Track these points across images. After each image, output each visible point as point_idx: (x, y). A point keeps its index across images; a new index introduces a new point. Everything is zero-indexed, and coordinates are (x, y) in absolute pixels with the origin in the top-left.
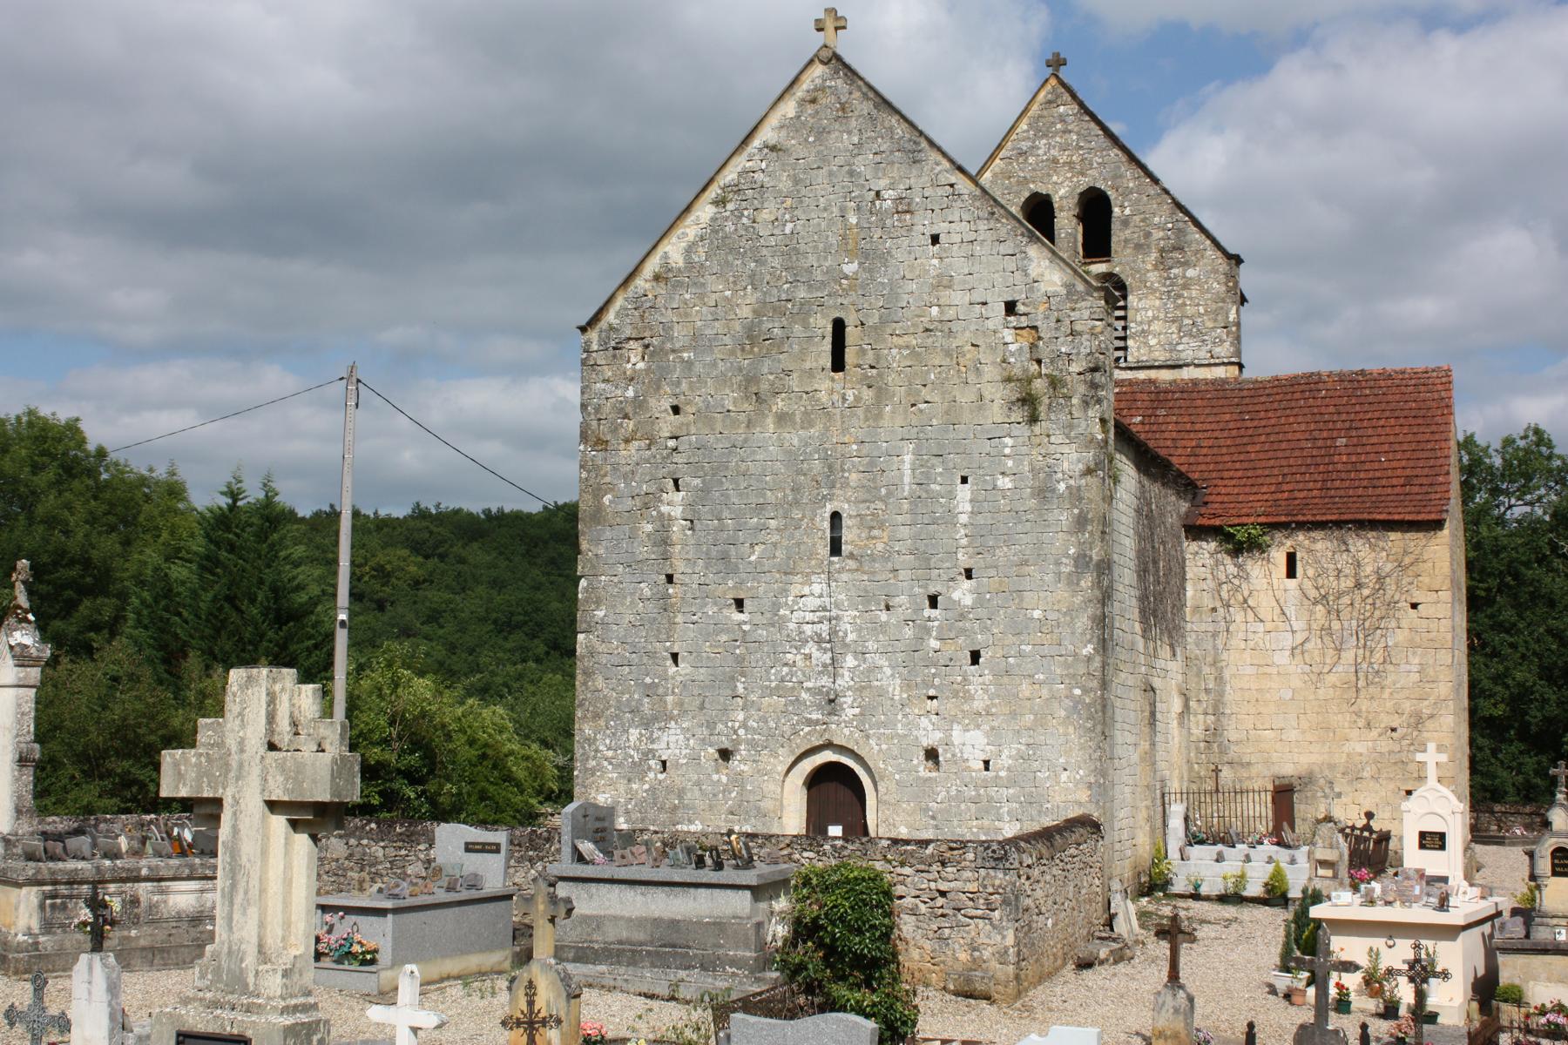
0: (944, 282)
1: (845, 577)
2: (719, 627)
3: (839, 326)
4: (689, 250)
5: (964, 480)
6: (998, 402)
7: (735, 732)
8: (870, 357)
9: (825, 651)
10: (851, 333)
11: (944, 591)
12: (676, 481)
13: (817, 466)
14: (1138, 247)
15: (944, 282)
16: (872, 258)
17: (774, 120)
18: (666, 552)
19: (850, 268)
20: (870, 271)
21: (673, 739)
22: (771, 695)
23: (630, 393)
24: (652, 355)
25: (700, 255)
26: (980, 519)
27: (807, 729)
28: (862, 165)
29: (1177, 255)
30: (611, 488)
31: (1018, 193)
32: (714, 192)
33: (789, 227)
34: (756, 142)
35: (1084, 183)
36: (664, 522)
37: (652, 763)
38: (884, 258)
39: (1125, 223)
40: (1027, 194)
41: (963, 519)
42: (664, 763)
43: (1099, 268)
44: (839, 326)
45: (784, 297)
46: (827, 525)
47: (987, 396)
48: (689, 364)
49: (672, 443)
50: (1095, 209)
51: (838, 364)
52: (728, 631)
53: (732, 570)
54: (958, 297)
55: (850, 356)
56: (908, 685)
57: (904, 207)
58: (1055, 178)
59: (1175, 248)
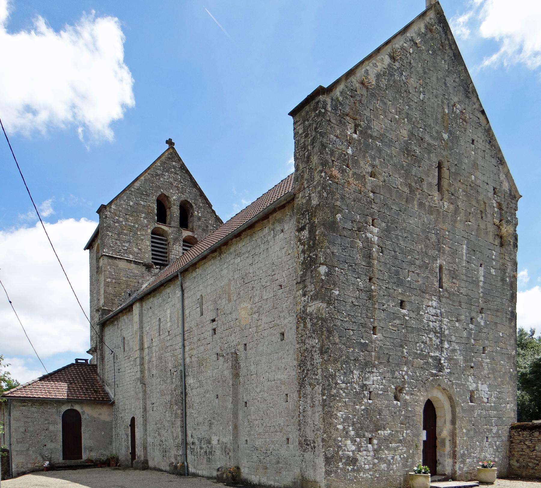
2: (395, 316)
4: (378, 76)
9: (438, 337)
11: (475, 316)
13: (434, 238)
21: (375, 378)
22: (417, 358)
24: (361, 132)
27: (431, 378)
28: (450, 81)
30: (340, 211)
31: (156, 191)
32: (388, 49)
34: (408, 34)
35: (183, 197)
36: (368, 242)
37: (365, 392)
39: (199, 219)
40: (160, 193)
41: (481, 284)
43: (186, 233)
46: (438, 270)
48: (380, 150)
50: (185, 210)
52: (399, 318)
53: (400, 283)
55: (445, 183)
56: (466, 361)
58: (171, 191)
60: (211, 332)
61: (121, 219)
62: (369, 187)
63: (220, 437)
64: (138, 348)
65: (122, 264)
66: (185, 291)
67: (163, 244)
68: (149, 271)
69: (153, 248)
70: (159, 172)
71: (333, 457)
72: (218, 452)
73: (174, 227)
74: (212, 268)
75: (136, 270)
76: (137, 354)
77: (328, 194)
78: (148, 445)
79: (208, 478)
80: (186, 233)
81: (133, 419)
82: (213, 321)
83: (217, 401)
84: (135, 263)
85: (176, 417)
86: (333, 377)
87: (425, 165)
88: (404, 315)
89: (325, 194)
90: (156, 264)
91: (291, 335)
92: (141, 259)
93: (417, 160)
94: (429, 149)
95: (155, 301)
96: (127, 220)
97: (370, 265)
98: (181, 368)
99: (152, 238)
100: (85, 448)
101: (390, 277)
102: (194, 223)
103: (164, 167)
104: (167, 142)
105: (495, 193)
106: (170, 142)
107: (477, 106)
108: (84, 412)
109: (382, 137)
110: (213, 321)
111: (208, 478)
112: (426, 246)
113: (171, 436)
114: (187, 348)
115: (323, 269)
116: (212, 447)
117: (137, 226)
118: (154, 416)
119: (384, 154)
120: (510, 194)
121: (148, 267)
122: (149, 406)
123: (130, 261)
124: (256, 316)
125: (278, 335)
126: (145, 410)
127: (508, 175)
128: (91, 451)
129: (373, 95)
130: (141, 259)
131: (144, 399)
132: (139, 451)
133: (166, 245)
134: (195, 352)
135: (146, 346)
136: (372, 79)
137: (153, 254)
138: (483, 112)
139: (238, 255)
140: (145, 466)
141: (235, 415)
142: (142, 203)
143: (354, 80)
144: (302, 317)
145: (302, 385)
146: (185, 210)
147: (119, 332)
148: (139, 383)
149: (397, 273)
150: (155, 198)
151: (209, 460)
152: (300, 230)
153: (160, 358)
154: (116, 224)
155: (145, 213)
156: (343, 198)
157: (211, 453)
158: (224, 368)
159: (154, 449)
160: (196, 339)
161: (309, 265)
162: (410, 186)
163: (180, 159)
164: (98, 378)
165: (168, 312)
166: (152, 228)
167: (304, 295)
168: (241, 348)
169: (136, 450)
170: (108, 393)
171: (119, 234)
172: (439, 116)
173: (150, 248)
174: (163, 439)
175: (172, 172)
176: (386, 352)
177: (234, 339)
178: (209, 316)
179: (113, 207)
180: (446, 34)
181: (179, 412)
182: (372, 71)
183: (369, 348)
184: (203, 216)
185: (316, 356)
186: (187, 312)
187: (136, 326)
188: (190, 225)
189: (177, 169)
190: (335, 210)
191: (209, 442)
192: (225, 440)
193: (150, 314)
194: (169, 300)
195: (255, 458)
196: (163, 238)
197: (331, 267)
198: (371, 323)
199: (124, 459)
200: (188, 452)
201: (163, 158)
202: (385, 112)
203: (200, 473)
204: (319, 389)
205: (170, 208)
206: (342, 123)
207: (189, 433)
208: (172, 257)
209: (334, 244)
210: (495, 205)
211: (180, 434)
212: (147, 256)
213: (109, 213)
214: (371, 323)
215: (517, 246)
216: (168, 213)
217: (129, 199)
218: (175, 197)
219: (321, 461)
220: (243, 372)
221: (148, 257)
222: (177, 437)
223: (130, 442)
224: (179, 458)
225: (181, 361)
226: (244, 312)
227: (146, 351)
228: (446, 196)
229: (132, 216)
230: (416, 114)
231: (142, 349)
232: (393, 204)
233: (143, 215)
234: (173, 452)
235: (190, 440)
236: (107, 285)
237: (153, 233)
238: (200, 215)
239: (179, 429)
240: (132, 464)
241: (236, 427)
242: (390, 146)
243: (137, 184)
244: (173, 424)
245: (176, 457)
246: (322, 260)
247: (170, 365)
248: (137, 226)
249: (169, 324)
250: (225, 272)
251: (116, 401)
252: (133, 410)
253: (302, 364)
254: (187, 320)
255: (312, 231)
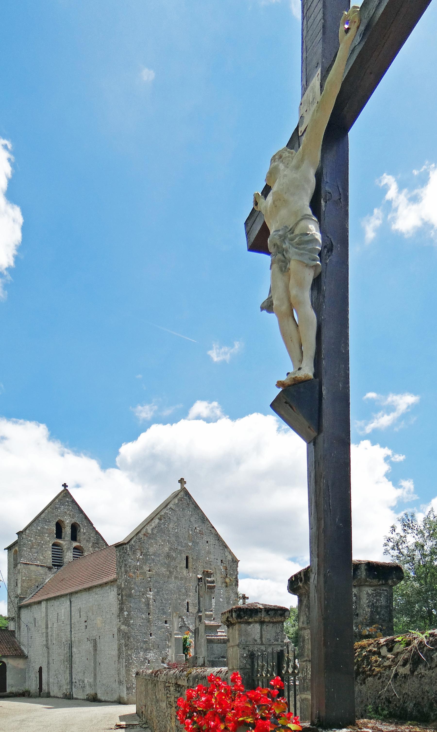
0: (209, 553)
1: (190, 617)
3: (187, 558)
4: (152, 529)
5: (213, 598)
6: (220, 582)
7: (167, 653)
8: (195, 567)
10: (190, 560)
12: (150, 589)
13: (184, 591)
14: (87, 541)
15: (209, 553)
16: (195, 543)
17: (173, 502)
18: (148, 607)
19: (190, 544)
20: (194, 546)
21: (151, 655)
23: (138, 564)
24: (144, 555)
25: (155, 531)
26: (217, 607)
28: (193, 519)
29: (96, 545)
30: (134, 589)
32: (158, 516)
33: (176, 530)
34: (168, 507)
35: (73, 521)
36: (148, 599)
38: (198, 543)
39: (84, 534)
40: (58, 520)
42: (149, 661)
43: (75, 544)
44: (187, 558)
45: (176, 547)
46: (186, 605)
47: (218, 580)
48: (153, 560)
49: (149, 579)
50: (74, 528)
51: (187, 567)
52: (164, 628)
53: (164, 613)
54: (212, 556)
55: (190, 565)
57: (201, 533)
59: (96, 543)
60: (84, 627)
61: (32, 539)
62: (148, 576)
63: (88, 680)
64: (44, 627)
65: (33, 568)
66: (72, 603)
67: (59, 552)
68: (50, 571)
69: (53, 555)
70: (57, 506)
71: (130, 687)
72: (87, 687)
73: (67, 541)
74: (85, 596)
75: (41, 571)
76: (44, 630)
77: (128, 583)
78: (50, 683)
79: (83, 700)
80: (75, 544)
81: (41, 669)
82: (86, 621)
83: (87, 661)
84: (41, 566)
85: (66, 668)
86: (130, 655)
87: (178, 560)
88: (167, 627)
89: (126, 584)
90: (54, 565)
91: (116, 636)
92: (45, 563)
93: (174, 559)
94: (181, 552)
95: (56, 603)
96: (36, 539)
97: (148, 608)
98: (69, 642)
99: (52, 548)
100: (9, 685)
101: (159, 612)
102: (80, 536)
103: (61, 503)
104: (63, 485)
105: (222, 563)
106: (65, 485)
107: (210, 525)
108: (8, 663)
109: (154, 554)
110: (86, 621)
111: (83, 700)
112: (179, 595)
113: (64, 679)
114: (73, 633)
115: (126, 613)
116: (85, 685)
117: (42, 542)
118: (54, 667)
119: (155, 561)
120: (233, 561)
121: (50, 568)
122: (51, 661)
123: (38, 565)
124: (104, 624)
125: (112, 635)
126: (48, 663)
127: (230, 552)
128: (12, 687)
129: (150, 538)
130: (45, 563)
131: (48, 657)
132: (44, 687)
133: (61, 552)
134: (77, 635)
135: (49, 626)
136: (150, 531)
137: (53, 559)
138: (213, 527)
139: (96, 594)
140: (48, 695)
141: (95, 669)
142: (46, 527)
143: (141, 535)
144: (119, 630)
145: (119, 658)
146: (74, 528)
147: (32, 614)
148: (45, 647)
149: (163, 609)
150: (54, 523)
151: (83, 691)
152: (119, 595)
153: (58, 635)
154: (29, 542)
155: (48, 534)
156: (135, 583)
157: (84, 687)
158: (89, 646)
159: (54, 686)
160: (77, 629)
161: (121, 610)
162: (170, 571)
163: (71, 496)
164: (16, 640)
165: (63, 610)
166: (53, 543)
167: (120, 622)
168: (98, 637)
169: (43, 686)
170: (23, 651)
171: (31, 549)
172: (187, 536)
173: (51, 556)
174: (59, 680)
175: (66, 505)
176: (157, 643)
177: (95, 633)
178: (84, 619)
179: (27, 531)
180: (190, 499)
181: (68, 666)
182: (149, 529)
183: (148, 643)
184: (87, 532)
185: (124, 647)
186: (73, 614)
187: (44, 615)
188: (78, 538)
189: (70, 503)
190: (131, 589)
191: (83, 682)
192: (90, 681)
193: (52, 609)
194: (63, 604)
195: (103, 689)
196: (58, 548)
197: (129, 612)
198: (149, 632)
199: (34, 692)
200: (73, 687)
201: (60, 496)
202: (156, 543)
203: (79, 697)
204: (124, 660)
205: (65, 528)
206: (134, 553)
207: (73, 678)
208: (65, 560)
209: (131, 602)
210: (222, 568)
211: (69, 677)
212: (49, 561)
213: (25, 536)
214: (149, 632)
215: (238, 585)
216: (63, 531)
217: (38, 525)
218: (68, 522)
219: (125, 689)
220: (98, 649)
221: (49, 562)
222: (67, 679)
223: (38, 681)
224: (68, 690)
225: (69, 639)
226: (99, 621)
227: (49, 630)
228: (191, 570)
229: (39, 536)
230: (173, 539)
231: (47, 628)
232: (161, 580)
233: (47, 535)
234: (65, 687)
235: (74, 680)
236: (23, 581)
237: (53, 545)
238: (85, 531)
239: (68, 675)
240: (40, 694)
241: (95, 675)
242: (159, 557)
243: (43, 516)
244: (65, 672)
245: (66, 689)
246: (125, 609)
247: (64, 640)
248: (42, 542)
249: (63, 618)
250: (91, 600)
251: (29, 656)
252: (41, 662)
253: (119, 649)
254: (73, 618)
255: (122, 597)
